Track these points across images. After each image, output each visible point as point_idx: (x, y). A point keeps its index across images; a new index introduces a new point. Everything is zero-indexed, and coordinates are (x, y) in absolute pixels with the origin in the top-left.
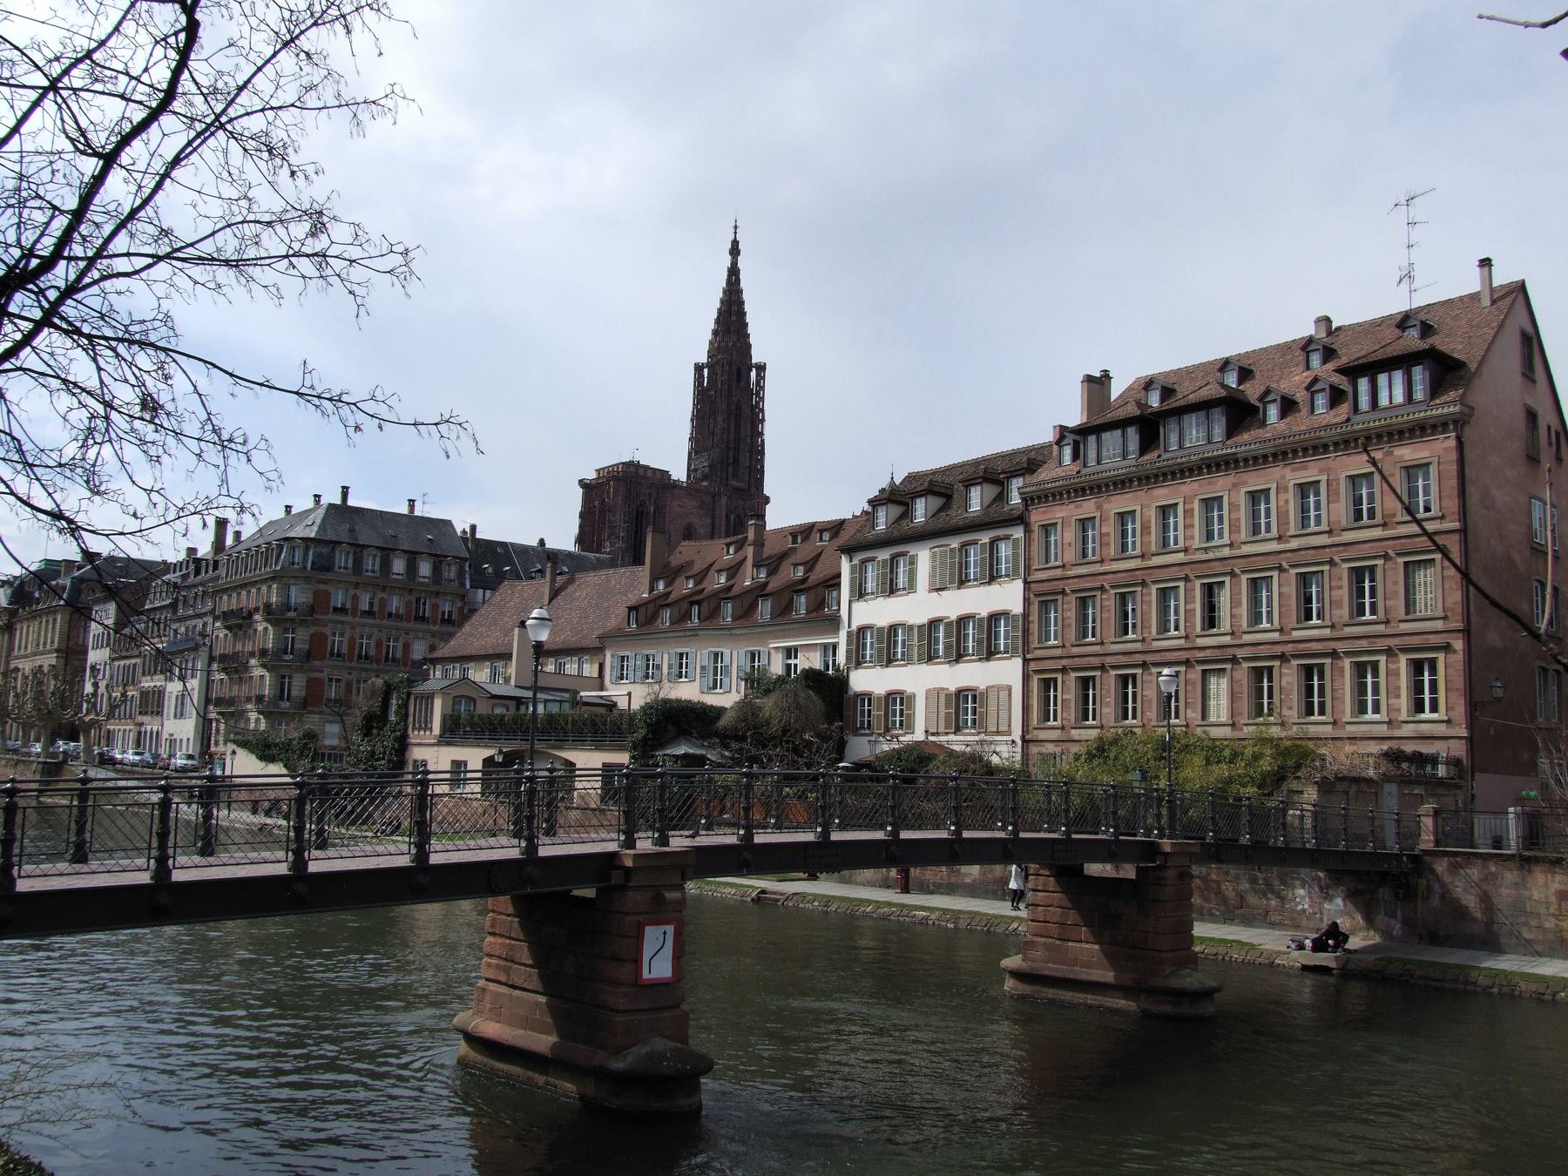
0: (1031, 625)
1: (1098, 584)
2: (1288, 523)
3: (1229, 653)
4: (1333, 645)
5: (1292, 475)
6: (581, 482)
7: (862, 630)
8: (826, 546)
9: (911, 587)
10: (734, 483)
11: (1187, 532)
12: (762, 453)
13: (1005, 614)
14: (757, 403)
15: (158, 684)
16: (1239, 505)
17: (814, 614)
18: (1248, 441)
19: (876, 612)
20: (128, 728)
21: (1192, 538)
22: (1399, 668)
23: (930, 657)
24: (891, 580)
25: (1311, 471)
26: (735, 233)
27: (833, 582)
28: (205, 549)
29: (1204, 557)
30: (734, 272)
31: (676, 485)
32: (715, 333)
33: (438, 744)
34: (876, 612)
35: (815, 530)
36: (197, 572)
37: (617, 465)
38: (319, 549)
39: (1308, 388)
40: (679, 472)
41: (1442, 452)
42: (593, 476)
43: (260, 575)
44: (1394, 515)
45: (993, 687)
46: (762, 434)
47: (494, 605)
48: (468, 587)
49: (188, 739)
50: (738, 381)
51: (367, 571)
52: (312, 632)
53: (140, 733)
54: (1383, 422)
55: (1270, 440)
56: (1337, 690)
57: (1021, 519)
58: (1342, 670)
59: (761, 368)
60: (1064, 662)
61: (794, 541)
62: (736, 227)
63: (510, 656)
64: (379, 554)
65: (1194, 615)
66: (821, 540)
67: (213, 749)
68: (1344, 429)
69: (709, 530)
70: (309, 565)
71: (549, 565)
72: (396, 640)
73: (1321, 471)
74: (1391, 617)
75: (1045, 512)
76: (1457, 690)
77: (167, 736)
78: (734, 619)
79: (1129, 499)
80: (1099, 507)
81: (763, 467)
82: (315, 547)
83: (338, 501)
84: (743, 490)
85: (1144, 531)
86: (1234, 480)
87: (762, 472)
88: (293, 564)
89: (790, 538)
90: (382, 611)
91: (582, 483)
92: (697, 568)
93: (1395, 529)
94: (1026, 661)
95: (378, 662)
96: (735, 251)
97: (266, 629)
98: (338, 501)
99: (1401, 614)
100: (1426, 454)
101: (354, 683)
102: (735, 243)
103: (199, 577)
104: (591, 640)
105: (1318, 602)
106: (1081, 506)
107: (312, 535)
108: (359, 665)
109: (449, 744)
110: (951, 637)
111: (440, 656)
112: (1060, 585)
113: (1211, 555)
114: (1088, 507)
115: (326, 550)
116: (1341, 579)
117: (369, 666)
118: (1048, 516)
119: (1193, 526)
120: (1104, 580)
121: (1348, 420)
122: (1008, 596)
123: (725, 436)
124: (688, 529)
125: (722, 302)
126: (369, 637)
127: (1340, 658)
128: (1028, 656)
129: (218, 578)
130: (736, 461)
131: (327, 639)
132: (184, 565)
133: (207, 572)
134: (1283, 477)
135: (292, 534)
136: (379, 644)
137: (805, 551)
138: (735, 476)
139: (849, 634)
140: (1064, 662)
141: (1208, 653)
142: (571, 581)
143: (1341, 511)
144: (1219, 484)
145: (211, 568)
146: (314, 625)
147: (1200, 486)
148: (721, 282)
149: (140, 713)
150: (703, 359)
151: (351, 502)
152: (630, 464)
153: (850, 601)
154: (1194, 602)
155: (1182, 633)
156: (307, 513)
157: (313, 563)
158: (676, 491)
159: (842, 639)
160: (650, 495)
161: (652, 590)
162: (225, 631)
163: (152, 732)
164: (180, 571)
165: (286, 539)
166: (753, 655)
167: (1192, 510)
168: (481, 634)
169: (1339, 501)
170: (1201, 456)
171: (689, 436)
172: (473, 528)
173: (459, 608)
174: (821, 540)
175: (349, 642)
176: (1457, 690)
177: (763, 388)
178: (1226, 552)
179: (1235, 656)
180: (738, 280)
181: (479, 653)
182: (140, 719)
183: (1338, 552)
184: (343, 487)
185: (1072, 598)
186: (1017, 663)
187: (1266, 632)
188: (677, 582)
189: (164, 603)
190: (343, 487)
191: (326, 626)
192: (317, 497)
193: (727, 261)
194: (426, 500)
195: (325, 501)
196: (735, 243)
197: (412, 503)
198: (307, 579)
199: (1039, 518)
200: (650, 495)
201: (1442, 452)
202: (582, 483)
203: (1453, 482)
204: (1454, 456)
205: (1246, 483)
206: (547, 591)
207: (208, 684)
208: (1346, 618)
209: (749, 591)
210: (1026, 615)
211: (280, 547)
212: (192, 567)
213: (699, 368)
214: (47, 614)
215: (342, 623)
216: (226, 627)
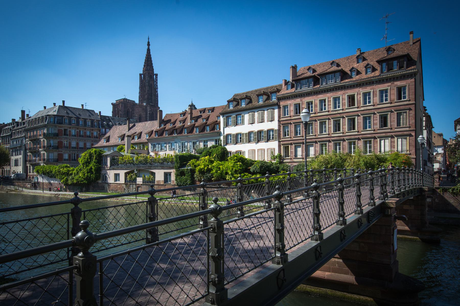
0: (281, 132)
1: (342, 116)
2: (361, 103)
3: (342, 138)
4: (374, 135)
5: (362, 90)
6: (112, 103)
7: (228, 135)
9: (243, 123)
10: (151, 104)
11: (330, 106)
12: (157, 96)
14: (156, 84)
16: (345, 99)
17: (212, 131)
18: (347, 81)
19: (232, 130)
21: (331, 108)
22: (395, 141)
23: (249, 141)
24: (236, 121)
25: (368, 89)
26: (149, 40)
27: (218, 123)
28: (18, 119)
29: (334, 113)
30: (149, 50)
32: (144, 66)
34: (232, 130)
35: (206, 110)
37: (121, 99)
38: (58, 118)
39: (365, 67)
40: (137, 101)
41: (410, 83)
42: (115, 102)
44: (394, 100)
45: (269, 149)
50: (151, 78)
54: (392, 75)
55: (354, 81)
56: (375, 147)
58: (377, 141)
59: (157, 75)
61: (201, 113)
62: (149, 38)
64: (76, 119)
65: (331, 128)
66: (209, 112)
67: (29, 174)
68: (380, 77)
70: (56, 122)
71: (128, 121)
73: (371, 89)
74: (392, 127)
75: (284, 102)
76: (413, 146)
77: (13, 171)
78: (187, 133)
79: (311, 98)
80: (301, 100)
82: (57, 117)
83: (62, 104)
85: (315, 107)
86: (344, 92)
87: (158, 101)
88: (51, 122)
91: (112, 104)
92: (172, 121)
93: (394, 104)
94: (279, 141)
96: (149, 44)
97: (44, 141)
98: (62, 104)
99: (396, 126)
100: (405, 83)
102: (149, 42)
103: (22, 126)
107: (56, 114)
108: (80, 150)
109: (114, 169)
110: (256, 136)
111: (97, 146)
112: (289, 122)
113: (336, 112)
114: (298, 101)
115: (60, 118)
116: (377, 117)
118: (337, 94)
119: (331, 105)
121: (380, 75)
122: (274, 125)
123: (148, 92)
124: (140, 115)
125: (146, 58)
127: (377, 139)
129: (25, 127)
130: (151, 99)
132: (12, 124)
133: (21, 125)
134: (359, 91)
135: (49, 114)
137: (205, 115)
138: (151, 103)
139: (224, 136)
141: (335, 138)
142: (134, 125)
143: (377, 99)
144: (339, 94)
146: (59, 139)
147: (333, 94)
148: (145, 52)
150: (142, 73)
151: (66, 105)
152: (125, 100)
153: (224, 128)
154: (331, 125)
155: (408, 126)
156: (53, 108)
157: (57, 122)
158: (137, 106)
159: (222, 138)
160: (130, 107)
162: (30, 142)
164: (21, 125)
165: (48, 115)
167: (331, 100)
169: (377, 97)
170: (334, 86)
171: (139, 92)
172: (100, 112)
173: (99, 134)
174: (209, 112)
176: (413, 146)
177: (157, 80)
178: (341, 111)
179: (344, 139)
180: (150, 52)
181: (109, 145)
183: (376, 111)
184: (63, 101)
185: (293, 125)
187: (325, 135)
188: (167, 125)
190: (63, 101)
191: (62, 139)
192: (55, 104)
193: (147, 47)
194: (86, 105)
195: (58, 105)
196: (149, 42)
197: (83, 105)
198: (56, 126)
200: (130, 107)
201: (410, 83)
202: (112, 104)
203: (413, 91)
204: (414, 83)
205: (347, 93)
206: (127, 128)
208: (378, 128)
209: (190, 126)
210: (279, 130)
213: (141, 75)
216: (30, 140)
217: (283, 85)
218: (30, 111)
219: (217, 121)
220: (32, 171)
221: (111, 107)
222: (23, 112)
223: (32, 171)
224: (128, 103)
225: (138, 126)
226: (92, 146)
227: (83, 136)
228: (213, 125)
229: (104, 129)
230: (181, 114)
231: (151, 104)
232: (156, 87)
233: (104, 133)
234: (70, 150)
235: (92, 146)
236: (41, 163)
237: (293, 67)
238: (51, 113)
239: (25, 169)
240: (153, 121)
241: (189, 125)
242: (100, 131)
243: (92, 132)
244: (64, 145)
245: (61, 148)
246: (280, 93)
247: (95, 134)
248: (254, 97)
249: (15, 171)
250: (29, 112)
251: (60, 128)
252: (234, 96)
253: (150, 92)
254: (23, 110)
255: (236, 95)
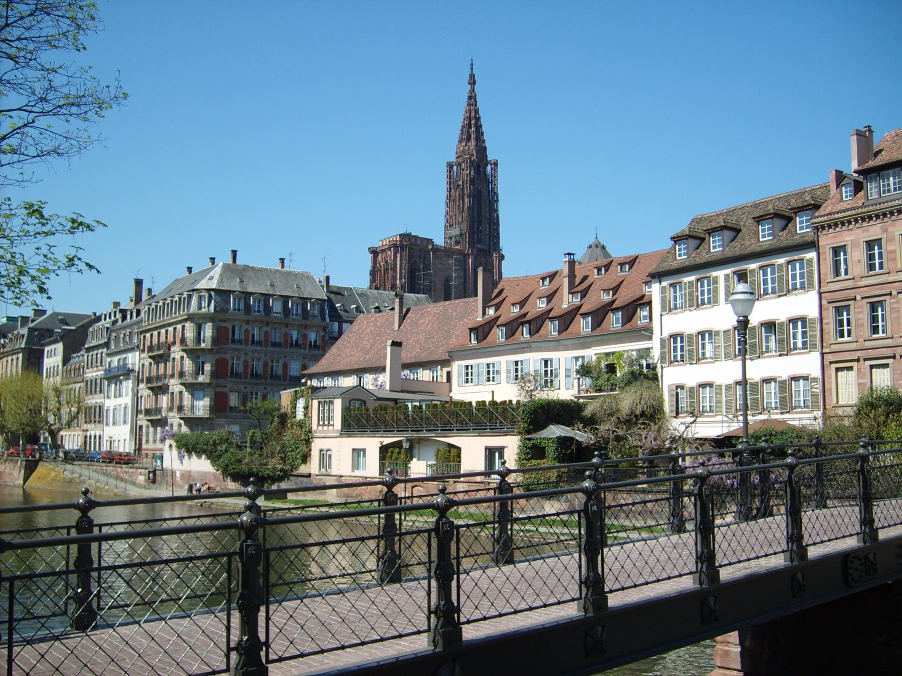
1: (888, 291)
8: (627, 275)
12: (497, 224)
13: (803, 320)
15: (98, 401)
20: (76, 433)
30: (472, 98)
31: (436, 249)
33: (341, 436)
36: (124, 318)
43: (175, 318)
46: (497, 211)
47: (354, 333)
48: (328, 320)
49: (125, 440)
51: (254, 312)
52: (217, 358)
53: (86, 437)
57: (812, 245)
59: (496, 164)
60: (859, 354)
62: (472, 64)
63: (383, 369)
67: (144, 446)
69: (463, 280)
72: (278, 361)
75: (835, 237)
77: (108, 438)
80: (885, 230)
81: (498, 234)
83: (230, 261)
84: (485, 251)
89: (596, 270)
90: (266, 340)
95: (265, 378)
96: (472, 82)
101: (249, 394)
102: (472, 76)
104: (441, 355)
105: (883, 321)
106: (868, 230)
107: (214, 287)
108: (252, 381)
110: (755, 338)
117: (258, 381)
118: (838, 239)
120: (892, 288)
126: (258, 360)
128: (824, 351)
131: (228, 363)
133: (131, 318)
136: (265, 365)
138: (479, 242)
139: (662, 341)
140: (859, 354)
145: (134, 315)
149: (86, 422)
150: (453, 159)
152: (405, 236)
160: (420, 257)
161: (484, 313)
163: (95, 437)
166: (546, 362)
168: (346, 355)
175: (244, 364)
182: (85, 426)
186: (816, 356)
189: (101, 342)
191: (227, 353)
192: (213, 260)
196: (472, 76)
199: (829, 242)
207: (137, 398)
211: (190, 297)
212: (119, 316)
213: (450, 166)
214: (12, 354)
215: (238, 350)
217: (833, 186)
218: (154, 280)
219: (643, 297)
220: (151, 439)
221: (367, 261)
222: (139, 283)
223: (151, 439)
224: (414, 247)
225: (424, 313)
226: (305, 372)
227: (240, 342)
228: (631, 308)
229: (336, 324)
230: (543, 279)
231: (479, 246)
232: (493, 198)
233: (335, 335)
234: (246, 383)
235: (305, 372)
236: (174, 417)
237: (859, 134)
238: (203, 284)
239: (137, 433)
240: (466, 300)
241: (480, 321)
242: (324, 329)
243: (304, 331)
244: (232, 368)
245: (224, 378)
246: (821, 211)
247: (312, 336)
248: (746, 223)
249: (114, 438)
250: (153, 282)
251: (223, 324)
252: (692, 222)
253: (476, 212)
254: (140, 278)
255: (698, 221)
